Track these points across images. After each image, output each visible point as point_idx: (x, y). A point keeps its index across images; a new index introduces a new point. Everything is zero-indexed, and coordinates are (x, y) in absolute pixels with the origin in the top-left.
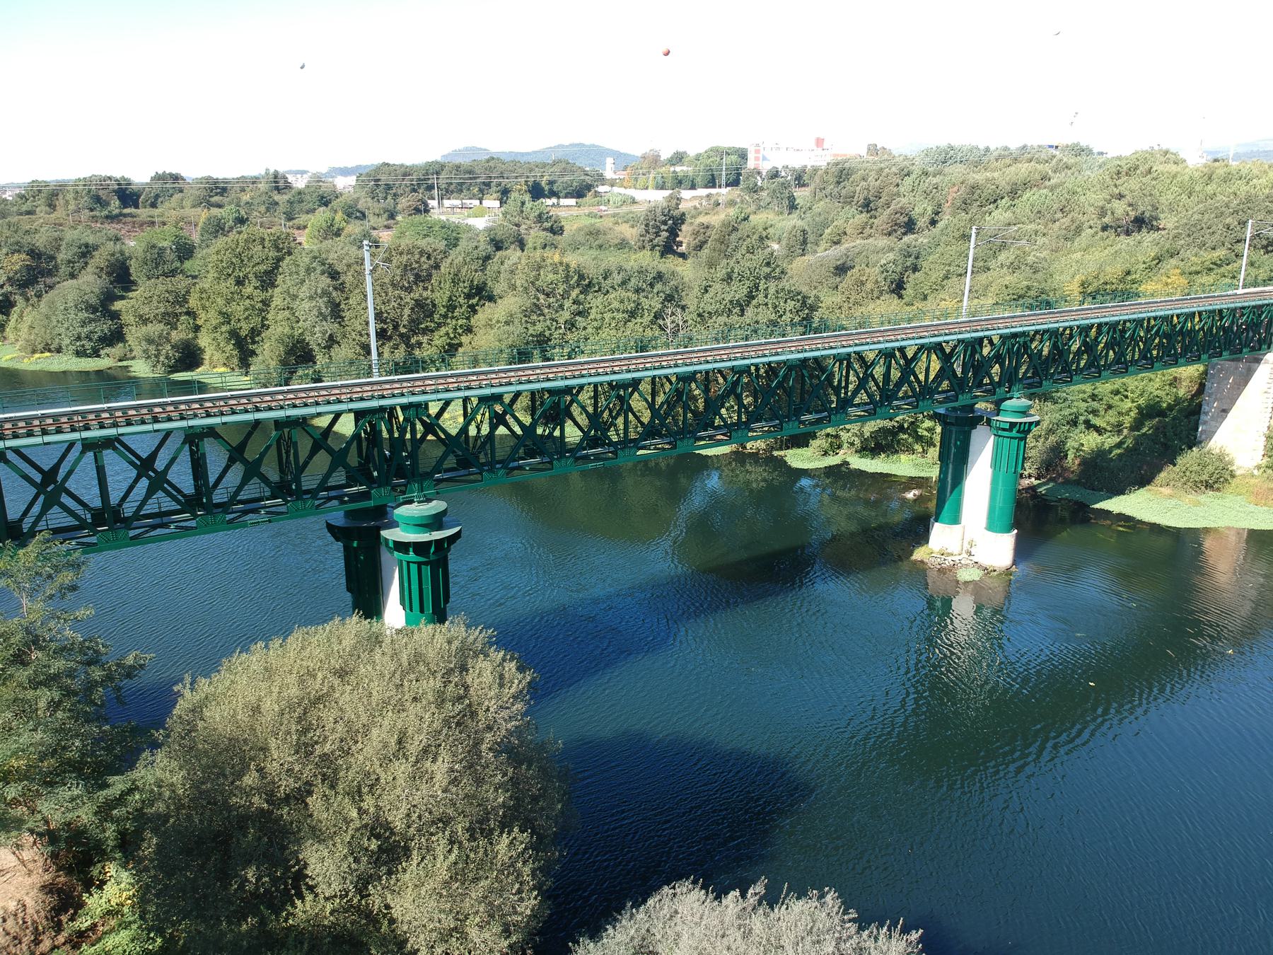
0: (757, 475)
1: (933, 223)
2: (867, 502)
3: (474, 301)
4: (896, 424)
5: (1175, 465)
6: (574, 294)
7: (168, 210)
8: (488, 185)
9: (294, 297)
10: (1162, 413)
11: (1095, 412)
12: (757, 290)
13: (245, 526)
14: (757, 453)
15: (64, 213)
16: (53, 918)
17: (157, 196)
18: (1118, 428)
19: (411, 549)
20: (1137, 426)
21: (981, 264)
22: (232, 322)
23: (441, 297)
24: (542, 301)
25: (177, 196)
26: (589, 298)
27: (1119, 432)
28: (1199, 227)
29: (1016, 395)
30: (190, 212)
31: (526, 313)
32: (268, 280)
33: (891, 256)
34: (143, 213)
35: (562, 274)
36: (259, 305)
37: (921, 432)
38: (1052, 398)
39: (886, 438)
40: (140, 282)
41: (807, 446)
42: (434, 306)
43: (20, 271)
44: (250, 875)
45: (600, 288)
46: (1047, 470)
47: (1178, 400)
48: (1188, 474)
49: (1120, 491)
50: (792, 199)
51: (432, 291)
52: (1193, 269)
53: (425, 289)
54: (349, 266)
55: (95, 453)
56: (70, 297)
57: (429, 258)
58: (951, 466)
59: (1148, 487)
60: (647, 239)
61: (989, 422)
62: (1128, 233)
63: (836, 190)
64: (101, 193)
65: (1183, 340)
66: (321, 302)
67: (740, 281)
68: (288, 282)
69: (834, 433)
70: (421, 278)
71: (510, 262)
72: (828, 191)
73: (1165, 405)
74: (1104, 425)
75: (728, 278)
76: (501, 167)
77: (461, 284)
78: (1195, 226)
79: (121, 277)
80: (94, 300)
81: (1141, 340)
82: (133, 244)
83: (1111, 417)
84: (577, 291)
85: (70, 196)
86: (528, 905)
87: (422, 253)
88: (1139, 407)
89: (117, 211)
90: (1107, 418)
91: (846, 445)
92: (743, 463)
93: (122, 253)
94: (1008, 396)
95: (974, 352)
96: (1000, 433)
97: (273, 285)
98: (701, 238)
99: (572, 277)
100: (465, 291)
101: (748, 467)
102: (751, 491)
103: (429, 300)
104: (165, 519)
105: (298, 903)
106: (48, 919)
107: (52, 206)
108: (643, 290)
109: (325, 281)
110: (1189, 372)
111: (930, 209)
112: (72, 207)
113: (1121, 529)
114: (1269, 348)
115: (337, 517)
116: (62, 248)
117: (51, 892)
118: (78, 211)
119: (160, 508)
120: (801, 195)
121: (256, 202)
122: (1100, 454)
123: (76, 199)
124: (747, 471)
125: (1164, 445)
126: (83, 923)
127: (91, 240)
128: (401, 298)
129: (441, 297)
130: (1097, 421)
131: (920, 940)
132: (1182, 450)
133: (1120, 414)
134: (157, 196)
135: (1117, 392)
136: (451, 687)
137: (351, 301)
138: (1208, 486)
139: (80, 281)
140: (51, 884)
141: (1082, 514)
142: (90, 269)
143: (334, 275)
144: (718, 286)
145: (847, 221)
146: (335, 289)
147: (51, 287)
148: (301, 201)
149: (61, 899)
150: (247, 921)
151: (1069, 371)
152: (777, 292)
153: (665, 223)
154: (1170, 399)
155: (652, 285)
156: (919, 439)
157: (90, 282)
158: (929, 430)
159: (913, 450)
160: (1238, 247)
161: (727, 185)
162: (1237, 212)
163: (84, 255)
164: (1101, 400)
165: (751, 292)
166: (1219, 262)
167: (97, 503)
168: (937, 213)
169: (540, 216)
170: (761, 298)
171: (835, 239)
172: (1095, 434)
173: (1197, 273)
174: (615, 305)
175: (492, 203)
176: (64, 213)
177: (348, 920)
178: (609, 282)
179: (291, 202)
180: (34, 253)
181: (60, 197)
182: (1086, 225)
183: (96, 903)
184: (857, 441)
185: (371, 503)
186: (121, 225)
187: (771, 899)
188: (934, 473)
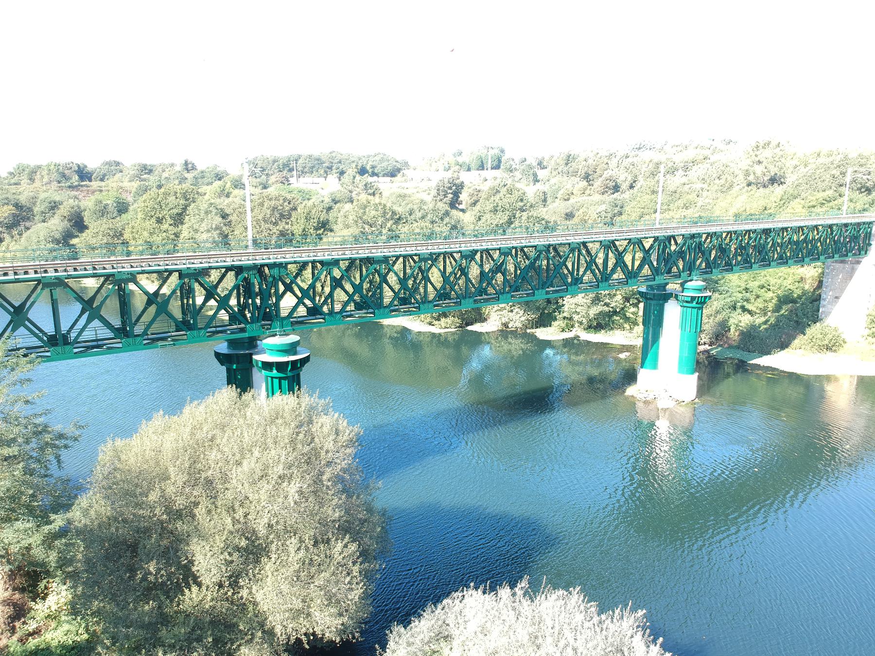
0: (516, 346)
1: (632, 187)
2: (592, 362)
3: (321, 232)
4: (611, 309)
5: (805, 335)
6: (389, 225)
7: (112, 183)
8: (330, 168)
9: (196, 231)
10: (794, 301)
11: (747, 300)
12: (514, 217)
13: (157, 347)
14: (516, 331)
15: (40, 184)
16: (9, 624)
17: (104, 175)
18: (764, 312)
19: (274, 368)
20: (777, 309)
21: (666, 207)
22: (153, 248)
23: (297, 229)
24: (367, 229)
25: (119, 175)
26: (399, 227)
27: (765, 314)
28: (814, 178)
29: (695, 278)
30: (126, 184)
31: (356, 239)
32: (179, 219)
33: (603, 207)
34: (95, 184)
35: (381, 211)
36: (173, 236)
37: (628, 314)
38: (718, 291)
39: (604, 319)
40: (90, 225)
41: (550, 326)
42: (293, 235)
43: (8, 217)
44: (151, 569)
45: (407, 221)
46: (717, 339)
47: (804, 293)
48: (814, 340)
49: (768, 353)
50: (535, 175)
51: (292, 225)
52: (811, 204)
53: (287, 223)
54: (234, 210)
55: (51, 290)
56: (42, 234)
57: (289, 203)
58: (651, 329)
59: (786, 350)
60: (438, 199)
61: (676, 297)
62: (764, 186)
63: (566, 168)
64: (66, 172)
65: (807, 246)
66: (215, 234)
67: (503, 211)
68: (192, 220)
69: (569, 316)
70: (285, 216)
71: (344, 211)
72: (560, 169)
73: (795, 295)
74: (754, 309)
75: (495, 211)
76: (339, 157)
77: (312, 220)
78: (810, 176)
79: (78, 223)
80: (58, 236)
81: (778, 246)
82: (88, 203)
83: (760, 304)
84: (391, 222)
85: (45, 173)
86: (356, 594)
87: (285, 200)
88: (778, 297)
89: (76, 183)
90: (756, 304)
91: (577, 325)
92: (506, 338)
93: (79, 207)
94: (689, 278)
95: (665, 247)
96: (685, 304)
97: (182, 223)
98: (475, 198)
99: (388, 213)
100: (315, 225)
101: (510, 340)
102: (512, 357)
103: (289, 231)
104: (100, 343)
105: (186, 591)
106: (5, 624)
107: (32, 180)
108: (436, 222)
109: (218, 220)
110: (809, 272)
111: (629, 178)
112: (46, 180)
113: (770, 376)
114: (866, 253)
115: (223, 348)
116: (38, 203)
117: (8, 605)
118: (50, 182)
119: (96, 334)
120: (542, 174)
121: (172, 177)
122: (753, 327)
123: (48, 174)
124: (510, 343)
125: (797, 322)
126: (32, 626)
127: (57, 198)
128: (270, 230)
129: (297, 229)
130: (749, 306)
131: (645, 616)
132: (809, 325)
133: (765, 301)
134: (104, 175)
135: (762, 287)
136: (301, 436)
137: (235, 233)
138: (828, 348)
139: (49, 224)
140: (8, 599)
141: (741, 366)
142: (56, 216)
143: (224, 216)
144: (488, 216)
145: (573, 186)
146: (225, 225)
147: (28, 229)
148: (203, 177)
149: (15, 611)
150: (148, 603)
151: (731, 265)
152: (528, 218)
153: (450, 188)
154: (799, 292)
155: (442, 219)
156: (627, 319)
157: (57, 224)
158: (633, 313)
159: (624, 328)
160: (842, 189)
161: (492, 168)
162: (839, 166)
163: (53, 208)
164: (752, 292)
165: (511, 219)
166: (828, 199)
167: (50, 329)
168: (635, 182)
169: (366, 185)
170: (517, 223)
171: (566, 198)
172: (749, 316)
173: (814, 207)
174: (417, 231)
175: (333, 178)
176: (40, 184)
177: (223, 607)
178: (413, 217)
179: (196, 178)
180: (17, 206)
181: (38, 173)
182: (736, 184)
183: (40, 609)
184: (585, 321)
185: (246, 335)
186: (79, 192)
187: (533, 592)
188: (639, 342)
